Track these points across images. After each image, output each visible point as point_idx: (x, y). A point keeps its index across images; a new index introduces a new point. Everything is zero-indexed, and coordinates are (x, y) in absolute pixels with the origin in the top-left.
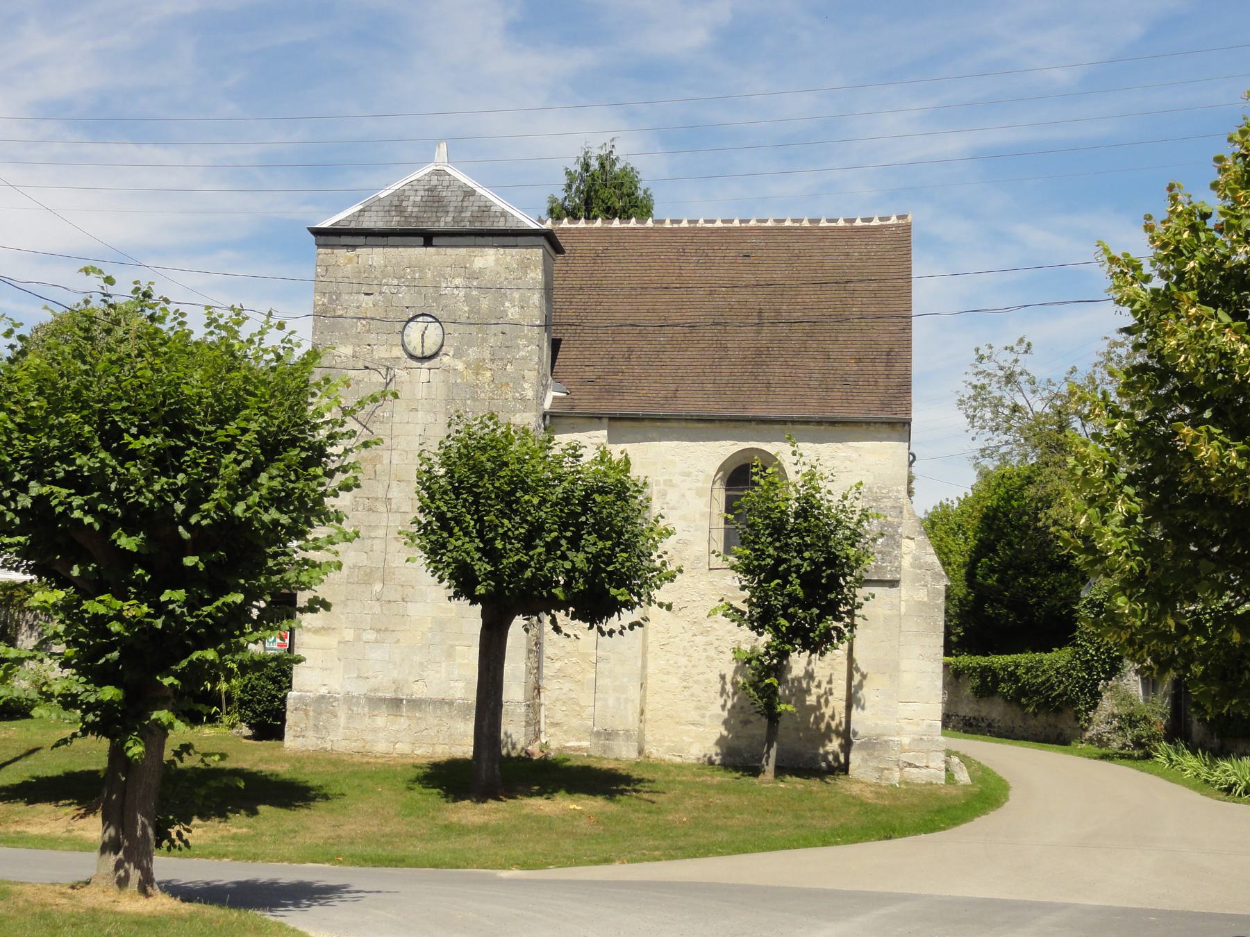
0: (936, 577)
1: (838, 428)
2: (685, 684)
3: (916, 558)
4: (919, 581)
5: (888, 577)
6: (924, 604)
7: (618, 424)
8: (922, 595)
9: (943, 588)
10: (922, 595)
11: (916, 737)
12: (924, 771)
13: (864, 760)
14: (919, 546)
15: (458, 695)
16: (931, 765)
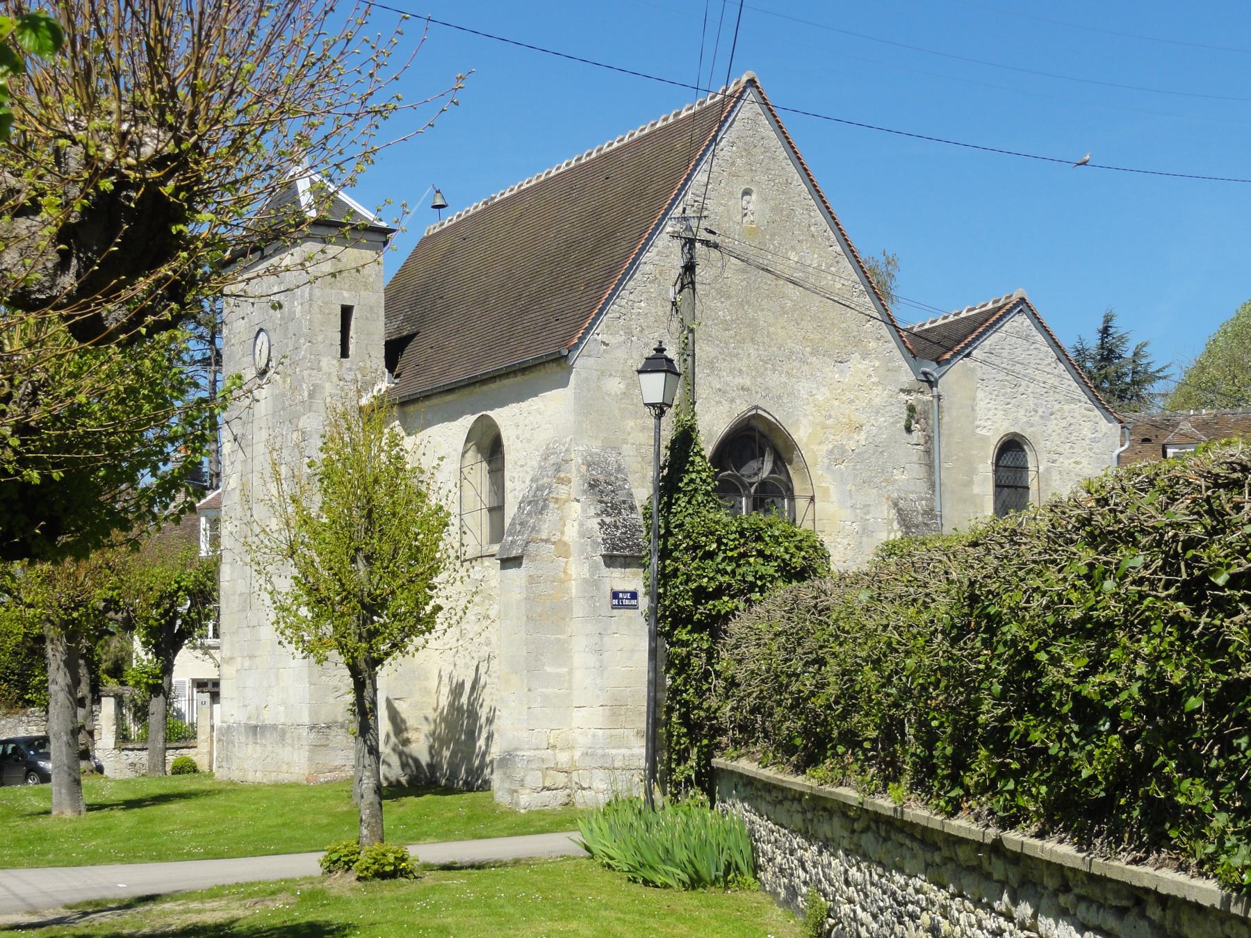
7: (411, 409)
13: (502, 781)
14: (584, 511)
15: (282, 720)
16: (594, 786)
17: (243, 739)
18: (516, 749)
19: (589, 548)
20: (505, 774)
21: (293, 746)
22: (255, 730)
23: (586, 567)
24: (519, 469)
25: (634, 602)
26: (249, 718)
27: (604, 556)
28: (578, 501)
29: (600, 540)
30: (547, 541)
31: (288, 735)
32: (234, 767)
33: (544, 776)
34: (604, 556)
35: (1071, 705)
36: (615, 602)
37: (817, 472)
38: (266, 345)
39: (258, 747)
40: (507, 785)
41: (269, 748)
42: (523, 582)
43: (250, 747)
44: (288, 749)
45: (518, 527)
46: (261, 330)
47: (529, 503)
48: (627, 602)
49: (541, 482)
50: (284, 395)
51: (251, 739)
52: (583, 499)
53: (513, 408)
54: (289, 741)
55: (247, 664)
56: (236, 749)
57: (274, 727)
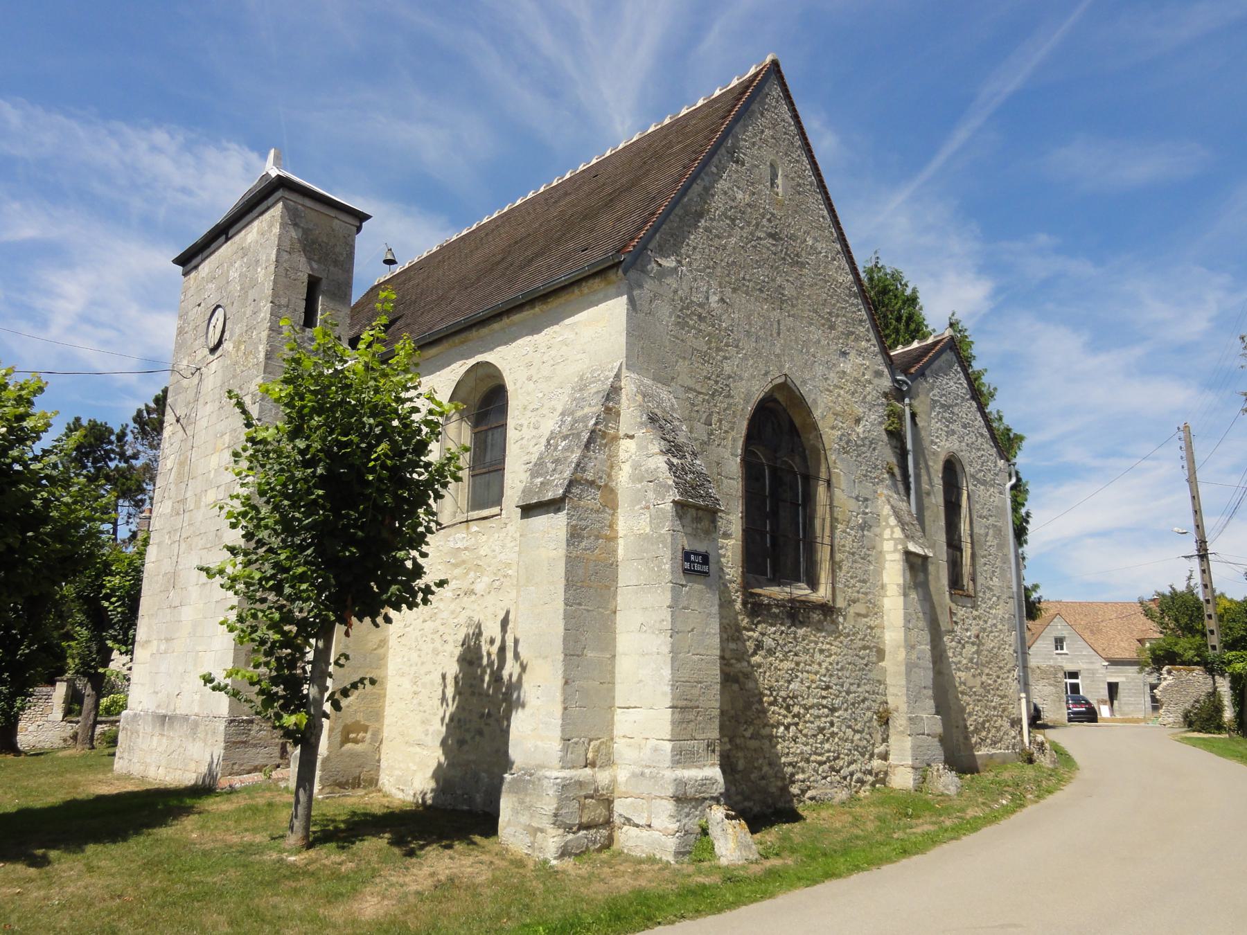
0: (662, 488)
1: (554, 303)
2: (415, 688)
3: (636, 466)
4: (639, 502)
5: (549, 496)
6: (644, 538)
8: (643, 525)
9: (668, 506)
10: (643, 525)
11: (638, 770)
12: (645, 833)
13: (516, 812)
14: (641, 447)
15: (196, 710)
16: (655, 823)
17: (149, 729)
18: (541, 767)
19: (651, 495)
20: (521, 802)
21: (205, 741)
22: (164, 720)
23: (646, 517)
24: (528, 414)
25: (705, 568)
26: (158, 706)
27: (674, 502)
28: (632, 437)
29: (671, 482)
30: (592, 483)
31: (202, 728)
32: (135, 760)
33: (583, 807)
34: (674, 502)
35: (89, 685)
36: (687, 565)
37: (832, 457)
38: (222, 320)
39: (164, 740)
40: (524, 819)
41: (177, 741)
42: (563, 534)
43: (155, 739)
44: (199, 744)
45: (551, 466)
46: (218, 306)
47: (565, 438)
48: (697, 567)
49: (579, 414)
50: (236, 363)
51: (157, 730)
52: (639, 433)
53: (524, 344)
54: (201, 735)
55: (163, 647)
56: (140, 740)
57: (186, 718)
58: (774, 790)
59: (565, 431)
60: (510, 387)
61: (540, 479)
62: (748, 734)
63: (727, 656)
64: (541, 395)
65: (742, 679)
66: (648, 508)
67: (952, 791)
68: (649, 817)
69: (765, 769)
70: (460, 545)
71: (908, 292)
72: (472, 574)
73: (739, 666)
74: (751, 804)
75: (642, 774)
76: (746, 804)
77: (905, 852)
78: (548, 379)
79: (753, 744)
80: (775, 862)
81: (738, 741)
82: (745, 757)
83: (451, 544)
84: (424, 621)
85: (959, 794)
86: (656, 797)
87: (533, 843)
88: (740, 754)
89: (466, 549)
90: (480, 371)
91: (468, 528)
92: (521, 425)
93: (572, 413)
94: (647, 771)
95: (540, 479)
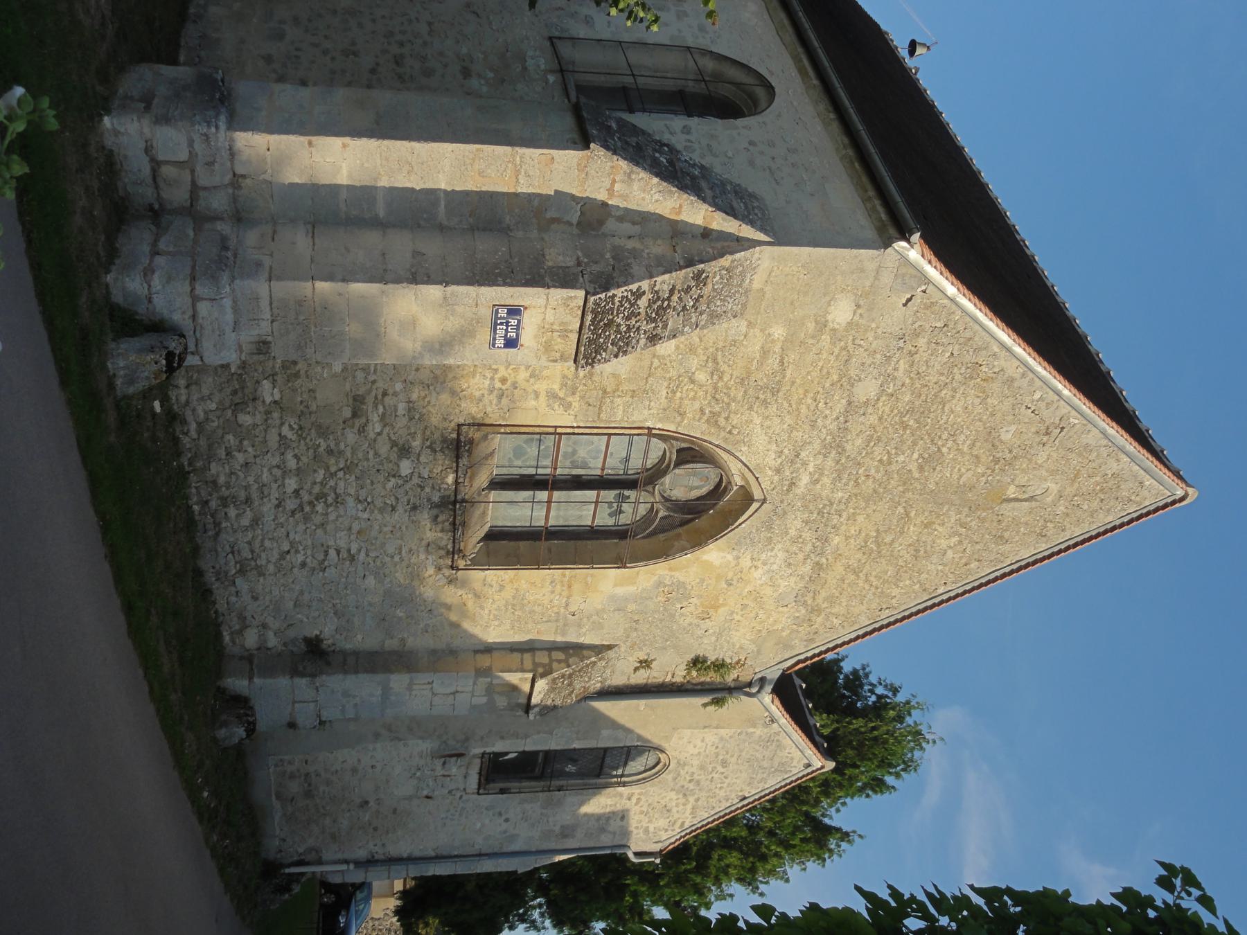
12: (146, 248)
25: (500, 342)
47: (670, 162)
58: (213, 471)
59: (679, 165)
60: (740, 122)
61: (614, 126)
62: (285, 430)
63: (388, 400)
64: (730, 154)
65: (358, 422)
66: (579, 264)
67: (222, 733)
68: (169, 253)
69: (240, 457)
70: (530, 63)
71: (890, 780)
72: (491, 75)
73: (376, 418)
74: (194, 434)
75: (226, 248)
76: (193, 426)
77: (128, 608)
78: (751, 163)
79: (273, 438)
80: (111, 418)
81: (276, 415)
82: (255, 426)
83: (530, 53)
84: (430, 24)
85: (215, 740)
86: (195, 262)
87: (132, 98)
88: (259, 418)
89: (525, 69)
90: (760, 92)
91: (552, 71)
92: (688, 133)
93: (704, 177)
94: (229, 254)
95: (614, 126)
